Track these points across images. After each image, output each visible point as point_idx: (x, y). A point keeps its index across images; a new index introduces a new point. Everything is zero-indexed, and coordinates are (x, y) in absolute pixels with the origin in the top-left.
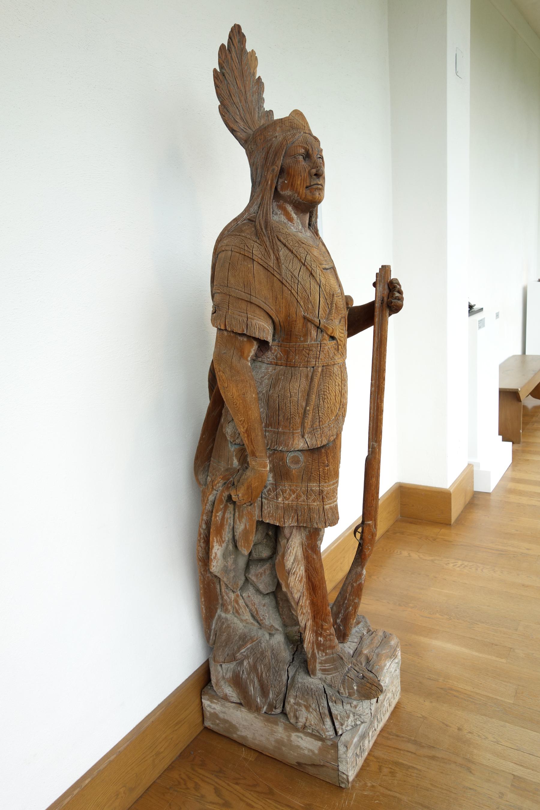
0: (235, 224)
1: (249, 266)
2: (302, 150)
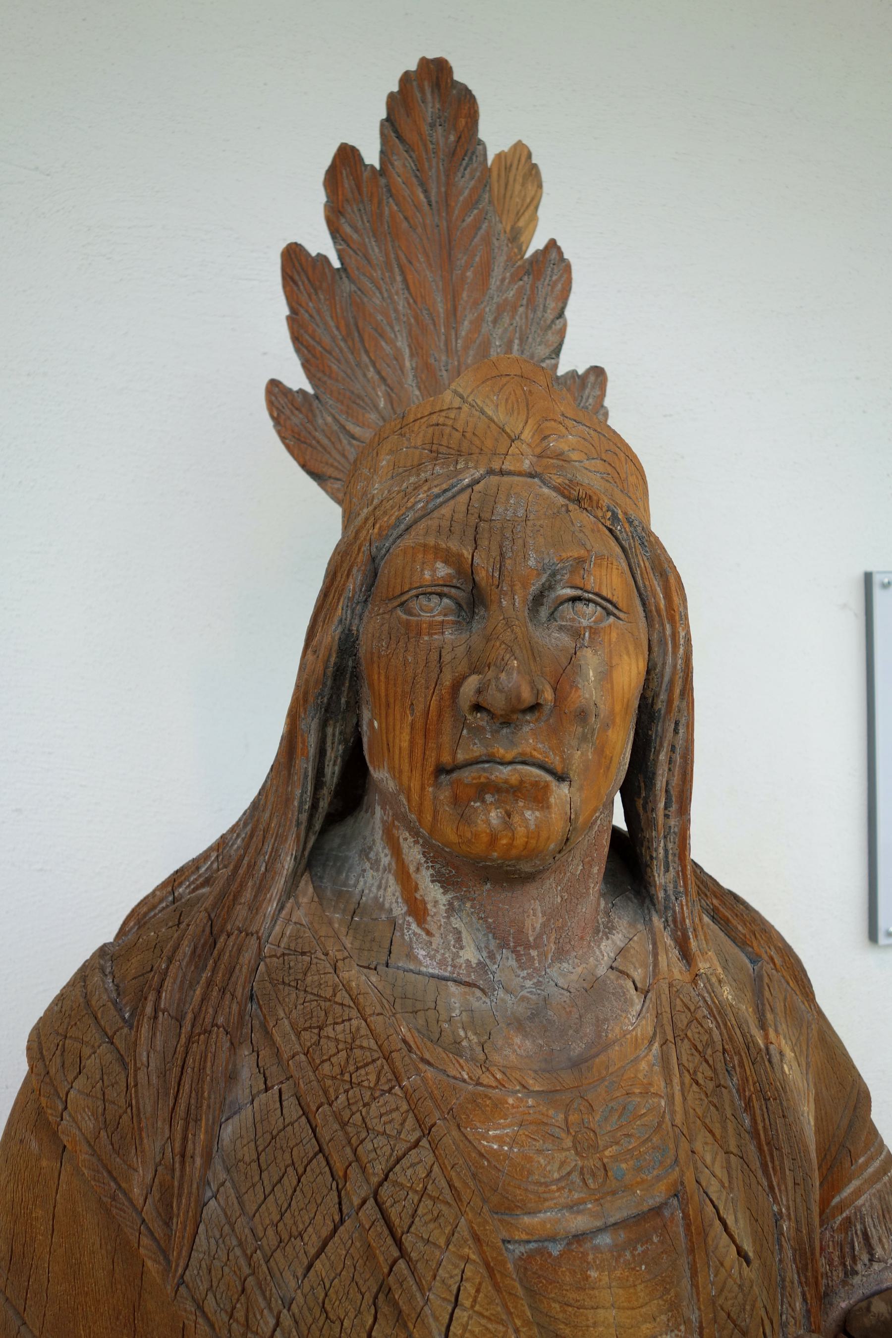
0: (166, 897)
1: (44, 1163)
2: (434, 570)
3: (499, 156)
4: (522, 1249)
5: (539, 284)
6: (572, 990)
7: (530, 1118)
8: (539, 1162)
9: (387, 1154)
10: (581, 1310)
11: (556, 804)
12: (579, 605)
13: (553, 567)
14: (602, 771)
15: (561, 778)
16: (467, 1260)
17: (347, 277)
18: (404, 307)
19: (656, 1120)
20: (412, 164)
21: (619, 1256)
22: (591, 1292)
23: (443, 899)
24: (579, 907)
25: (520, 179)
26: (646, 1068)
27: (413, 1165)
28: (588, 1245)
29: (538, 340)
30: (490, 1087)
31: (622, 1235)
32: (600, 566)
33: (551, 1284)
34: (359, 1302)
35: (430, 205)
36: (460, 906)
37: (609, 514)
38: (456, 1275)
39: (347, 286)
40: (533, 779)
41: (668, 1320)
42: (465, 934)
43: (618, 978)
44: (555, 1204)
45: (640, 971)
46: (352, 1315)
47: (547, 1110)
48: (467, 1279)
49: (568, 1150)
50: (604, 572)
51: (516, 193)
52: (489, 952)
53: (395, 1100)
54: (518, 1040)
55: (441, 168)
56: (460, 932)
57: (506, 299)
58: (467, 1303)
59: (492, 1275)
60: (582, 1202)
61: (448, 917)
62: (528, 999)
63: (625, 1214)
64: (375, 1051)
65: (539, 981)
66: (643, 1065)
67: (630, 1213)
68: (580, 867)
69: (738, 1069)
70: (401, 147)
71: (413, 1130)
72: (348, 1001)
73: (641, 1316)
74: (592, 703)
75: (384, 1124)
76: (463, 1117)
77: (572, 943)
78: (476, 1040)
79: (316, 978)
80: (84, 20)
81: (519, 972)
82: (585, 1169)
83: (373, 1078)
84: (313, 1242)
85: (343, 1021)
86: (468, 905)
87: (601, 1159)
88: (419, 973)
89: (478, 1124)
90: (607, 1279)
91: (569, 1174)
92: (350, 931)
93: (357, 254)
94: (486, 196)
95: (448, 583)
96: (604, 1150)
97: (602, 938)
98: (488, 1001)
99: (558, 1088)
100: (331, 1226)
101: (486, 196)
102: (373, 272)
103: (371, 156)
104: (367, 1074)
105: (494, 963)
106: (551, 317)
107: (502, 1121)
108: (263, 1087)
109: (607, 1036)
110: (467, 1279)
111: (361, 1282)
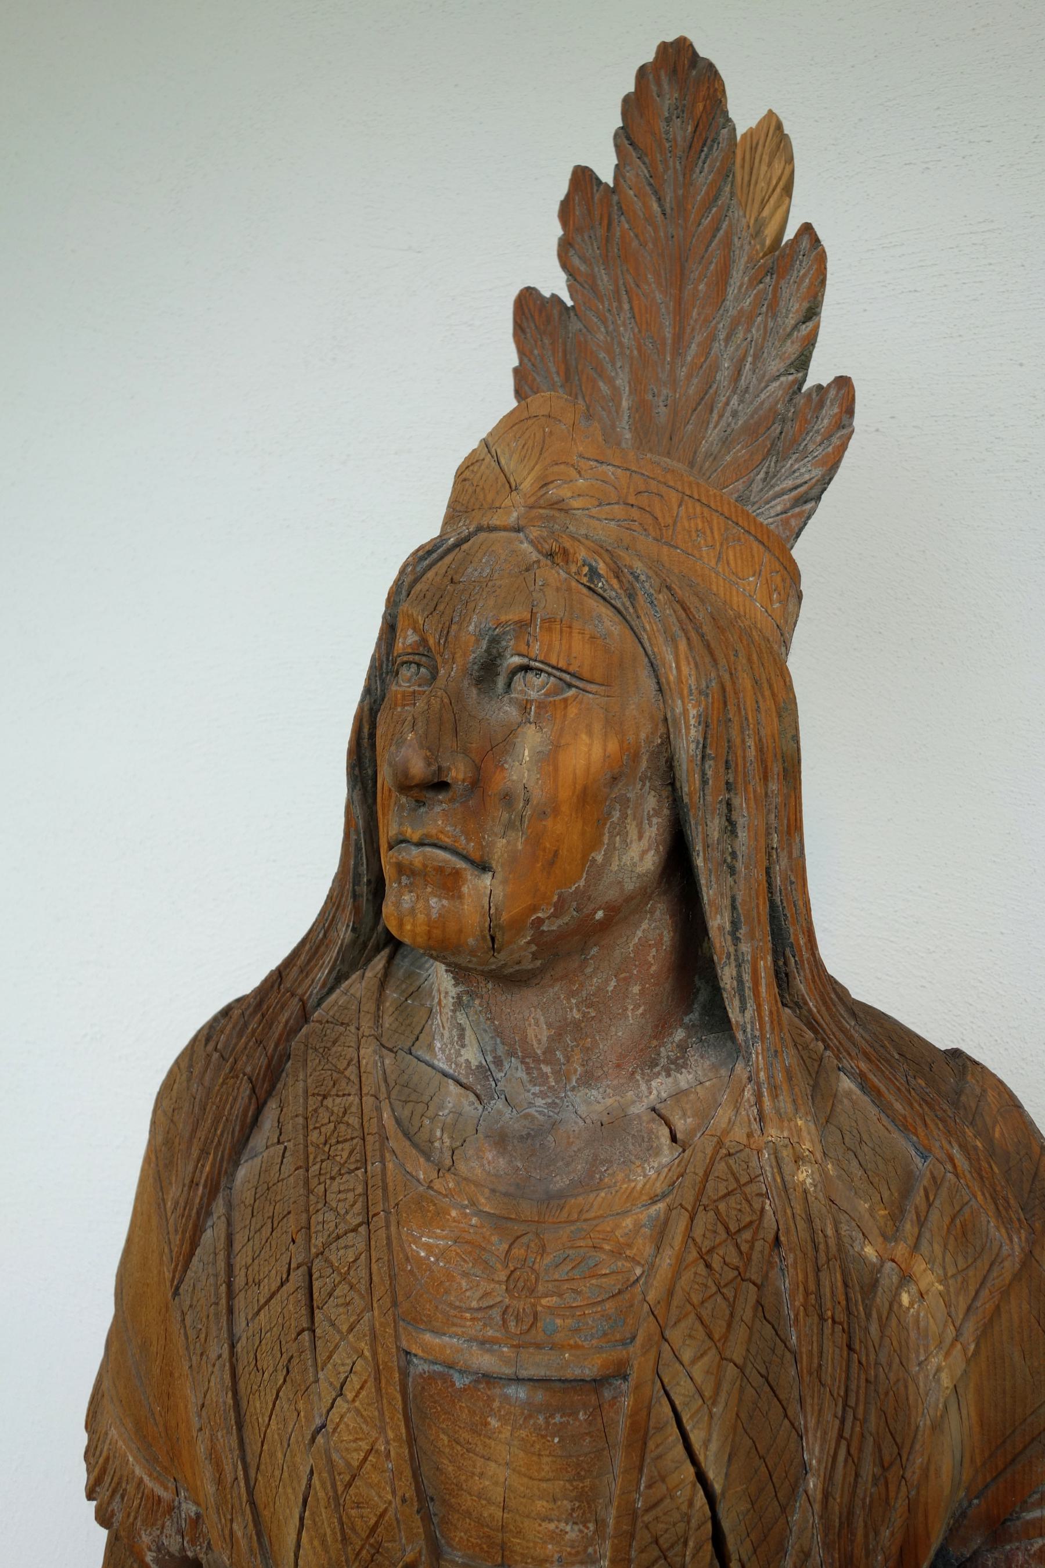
3: (744, 136)
4: (426, 1367)
5: (783, 283)
6: (587, 1121)
7: (468, 1237)
8: (460, 1284)
9: (331, 1229)
10: (471, 1454)
11: (470, 895)
12: (530, 675)
13: (490, 632)
14: (539, 865)
15: (483, 867)
16: (361, 1355)
17: (576, 315)
18: (629, 339)
19: (619, 1287)
20: (646, 171)
21: (530, 1416)
22: (487, 1441)
23: (453, 991)
24: (613, 1029)
25: (766, 158)
26: (631, 1226)
27: (346, 1247)
28: (498, 1391)
29: (774, 353)
30: (440, 1193)
31: (540, 1396)
32: (550, 630)
33: (445, 1413)
34: (278, 1359)
35: (665, 214)
36: (469, 1001)
37: (586, 569)
38: (348, 1365)
39: (575, 325)
40: (435, 863)
41: (573, 1510)
42: (468, 1033)
43: (653, 1120)
44: (463, 1333)
45: (689, 1120)
46: (271, 1369)
47: (492, 1234)
48: (355, 1373)
49: (499, 1282)
50: (556, 636)
51: (762, 176)
52: (495, 1057)
53: (354, 1182)
54: (489, 1156)
55: (678, 167)
56: (463, 1030)
57: (742, 308)
58: (350, 1396)
59: (378, 1380)
60: (493, 1341)
61: (454, 1011)
62: (533, 1118)
63: (543, 1374)
64: (356, 1130)
65: (554, 1103)
66: (628, 1222)
67: (548, 1373)
68: (613, 983)
69: (791, 1270)
70: (634, 154)
71: (358, 1214)
72: (354, 1078)
73: (539, 1489)
74: (521, 786)
75: (339, 1201)
76: (404, 1215)
77: (605, 1069)
78: (448, 1144)
79: (340, 1049)
80: (456, 86)
81: (529, 1087)
82: (511, 1310)
83: (345, 1155)
84: (265, 1291)
85: (344, 1095)
86: (477, 1002)
87: (534, 1305)
88: (433, 1067)
89: (414, 1227)
90: (509, 1434)
91: (491, 1307)
92: (396, 1013)
93: (584, 287)
94: (727, 189)
95: (416, 652)
96: (541, 1297)
97: (659, 1073)
98: (480, 1107)
99: (513, 1216)
100: (279, 1284)
101: (727, 189)
102: (599, 304)
103: (606, 175)
104: (342, 1150)
105: (500, 1070)
106: (793, 322)
107: (438, 1231)
108: (276, 1140)
109: (601, 1179)
110: (355, 1373)
111: (283, 1343)
